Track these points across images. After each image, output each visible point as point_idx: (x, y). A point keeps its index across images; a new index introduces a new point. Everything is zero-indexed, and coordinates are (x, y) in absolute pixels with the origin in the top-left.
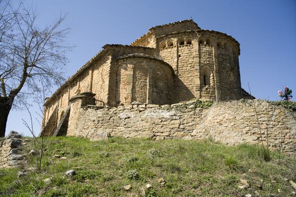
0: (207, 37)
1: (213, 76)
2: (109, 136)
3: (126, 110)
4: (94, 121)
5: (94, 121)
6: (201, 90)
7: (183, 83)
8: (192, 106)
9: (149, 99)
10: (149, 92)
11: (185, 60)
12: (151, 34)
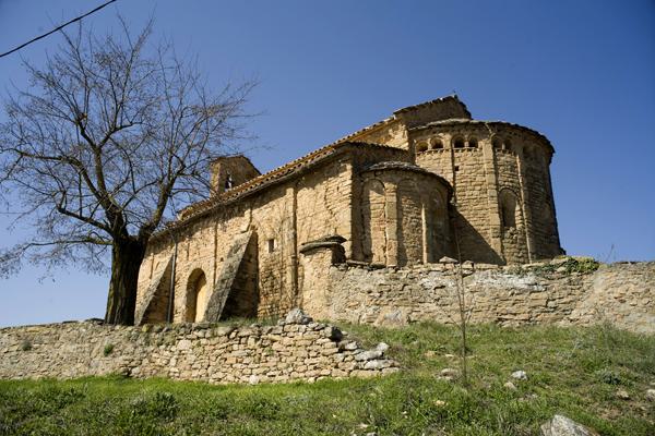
0: (507, 136)
1: (521, 210)
2: (409, 321)
3: (434, 273)
4: (370, 292)
5: (370, 292)
6: (502, 238)
7: (466, 222)
8: (562, 269)
9: (427, 252)
10: (427, 238)
11: (475, 176)
12: (397, 122)
